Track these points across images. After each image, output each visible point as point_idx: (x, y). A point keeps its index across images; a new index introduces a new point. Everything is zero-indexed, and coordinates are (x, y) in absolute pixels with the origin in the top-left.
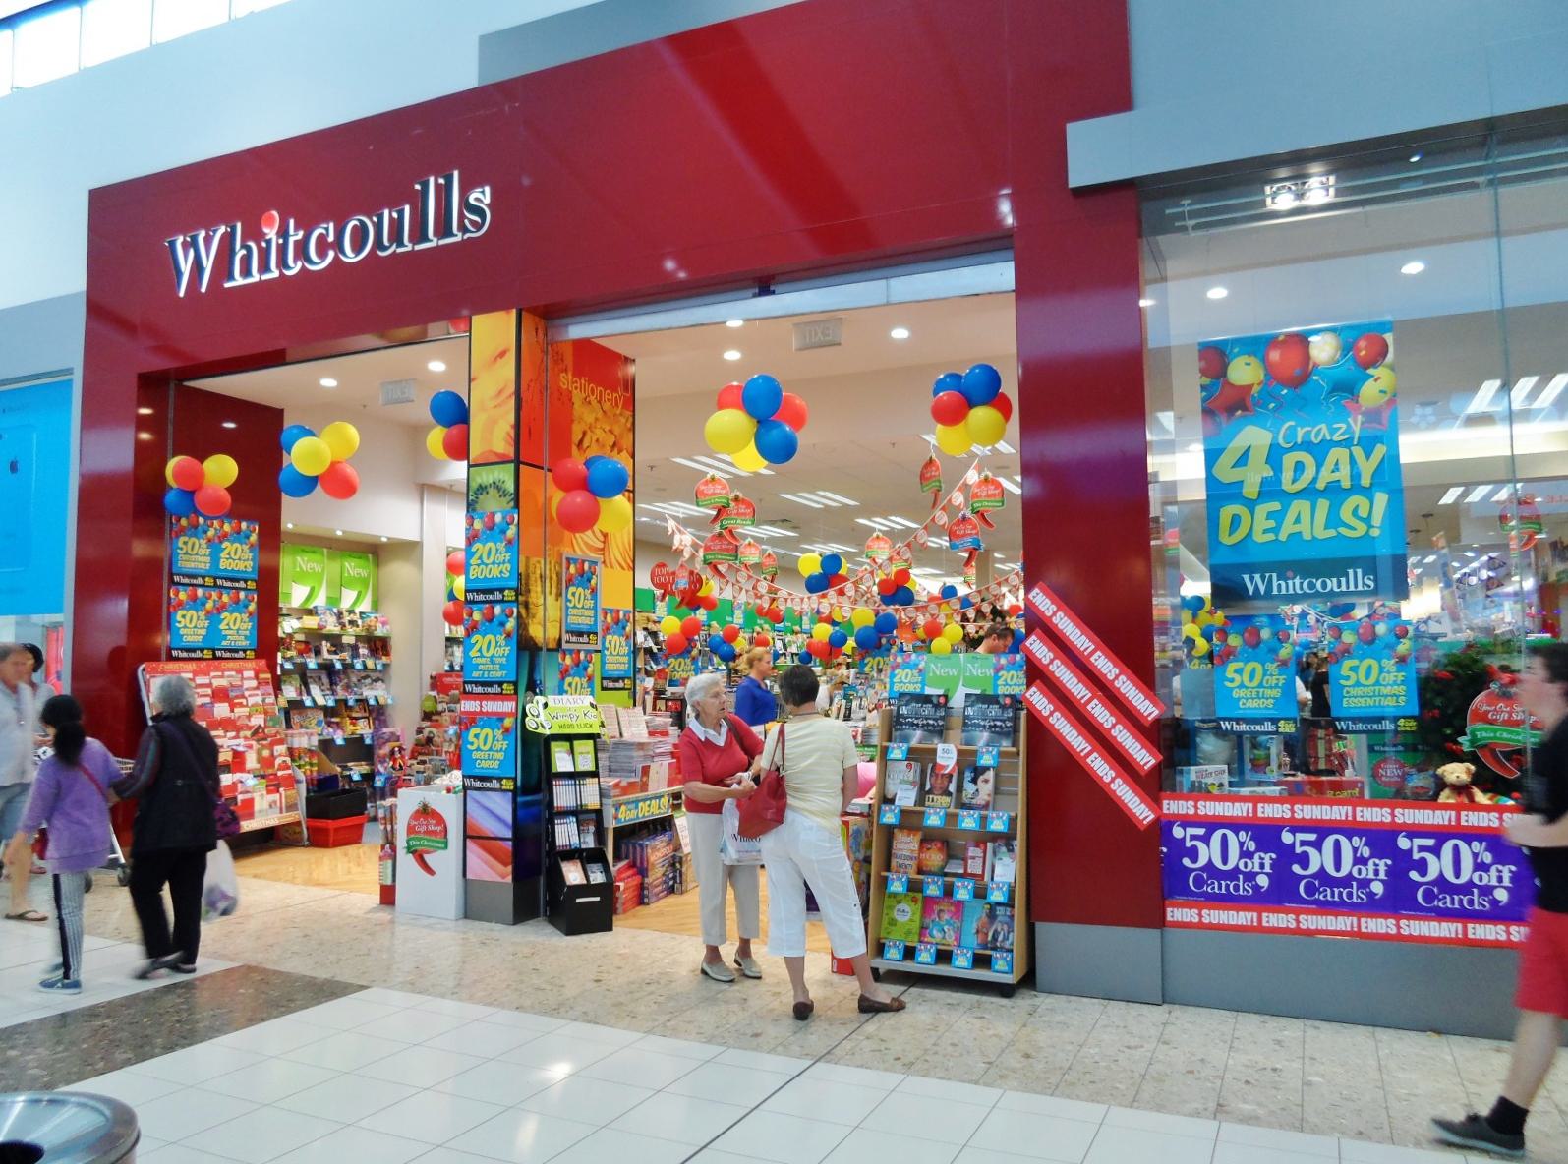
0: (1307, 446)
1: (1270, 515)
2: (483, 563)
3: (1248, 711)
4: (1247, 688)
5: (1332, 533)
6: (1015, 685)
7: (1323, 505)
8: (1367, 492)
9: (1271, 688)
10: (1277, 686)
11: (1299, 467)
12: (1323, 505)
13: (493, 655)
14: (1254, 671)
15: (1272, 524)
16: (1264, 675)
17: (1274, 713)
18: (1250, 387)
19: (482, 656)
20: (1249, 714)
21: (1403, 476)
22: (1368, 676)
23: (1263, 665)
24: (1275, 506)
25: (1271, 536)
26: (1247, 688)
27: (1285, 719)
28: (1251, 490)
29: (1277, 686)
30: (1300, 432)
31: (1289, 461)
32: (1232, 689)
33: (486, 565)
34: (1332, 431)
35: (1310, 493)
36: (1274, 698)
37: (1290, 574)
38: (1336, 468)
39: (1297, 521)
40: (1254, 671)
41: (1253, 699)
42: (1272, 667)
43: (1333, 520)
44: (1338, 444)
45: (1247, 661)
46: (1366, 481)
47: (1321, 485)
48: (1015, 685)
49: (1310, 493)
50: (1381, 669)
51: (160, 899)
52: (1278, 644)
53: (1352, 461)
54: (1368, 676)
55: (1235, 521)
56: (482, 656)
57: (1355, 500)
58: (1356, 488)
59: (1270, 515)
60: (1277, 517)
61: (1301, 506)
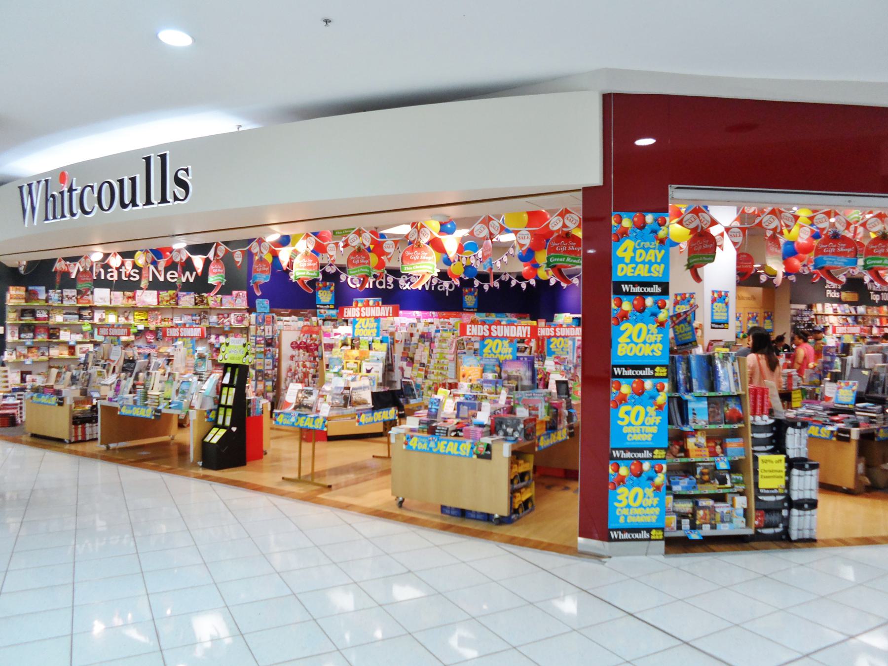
0: (643, 248)
1: (633, 268)
2: (632, 342)
3: (633, 443)
4: (633, 425)
5: (649, 275)
6: (644, 342)
7: (647, 266)
8: (659, 264)
9: (650, 426)
10: (654, 424)
11: (641, 255)
12: (647, 266)
13: (563, 348)
14: (638, 413)
15: (633, 271)
16: (646, 415)
17: (652, 445)
18: (628, 228)
19: (557, 348)
20: (634, 445)
21: (463, 216)
22: (637, 418)
23: (645, 408)
24: (634, 265)
25: (632, 275)
26: (633, 425)
27: (658, 448)
28: (627, 260)
29: (654, 424)
30: (642, 243)
31: (638, 252)
32: (623, 426)
33: (637, 344)
34: (651, 244)
35: (643, 262)
36: (653, 433)
37: (636, 285)
38: (651, 256)
39: (640, 270)
40: (638, 413)
41: (637, 433)
42: (652, 410)
43: (650, 271)
44: (652, 249)
45: (634, 404)
46: (659, 261)
47: (647, 260)
48: (644, 342)
49: (643, 262)
50: (647, 413)
51: (237, 382)
52: (657, 392)
53: (656, 255)
54: (637, 418)
55: (622, 269)
56: (557, 348)
57: (656, 266)
58: (656, 263)
59: (633, 268)
60: (634, 268)
61: (641, 266)
